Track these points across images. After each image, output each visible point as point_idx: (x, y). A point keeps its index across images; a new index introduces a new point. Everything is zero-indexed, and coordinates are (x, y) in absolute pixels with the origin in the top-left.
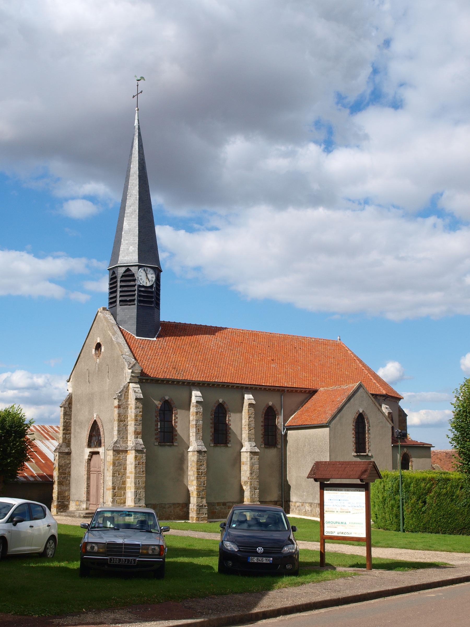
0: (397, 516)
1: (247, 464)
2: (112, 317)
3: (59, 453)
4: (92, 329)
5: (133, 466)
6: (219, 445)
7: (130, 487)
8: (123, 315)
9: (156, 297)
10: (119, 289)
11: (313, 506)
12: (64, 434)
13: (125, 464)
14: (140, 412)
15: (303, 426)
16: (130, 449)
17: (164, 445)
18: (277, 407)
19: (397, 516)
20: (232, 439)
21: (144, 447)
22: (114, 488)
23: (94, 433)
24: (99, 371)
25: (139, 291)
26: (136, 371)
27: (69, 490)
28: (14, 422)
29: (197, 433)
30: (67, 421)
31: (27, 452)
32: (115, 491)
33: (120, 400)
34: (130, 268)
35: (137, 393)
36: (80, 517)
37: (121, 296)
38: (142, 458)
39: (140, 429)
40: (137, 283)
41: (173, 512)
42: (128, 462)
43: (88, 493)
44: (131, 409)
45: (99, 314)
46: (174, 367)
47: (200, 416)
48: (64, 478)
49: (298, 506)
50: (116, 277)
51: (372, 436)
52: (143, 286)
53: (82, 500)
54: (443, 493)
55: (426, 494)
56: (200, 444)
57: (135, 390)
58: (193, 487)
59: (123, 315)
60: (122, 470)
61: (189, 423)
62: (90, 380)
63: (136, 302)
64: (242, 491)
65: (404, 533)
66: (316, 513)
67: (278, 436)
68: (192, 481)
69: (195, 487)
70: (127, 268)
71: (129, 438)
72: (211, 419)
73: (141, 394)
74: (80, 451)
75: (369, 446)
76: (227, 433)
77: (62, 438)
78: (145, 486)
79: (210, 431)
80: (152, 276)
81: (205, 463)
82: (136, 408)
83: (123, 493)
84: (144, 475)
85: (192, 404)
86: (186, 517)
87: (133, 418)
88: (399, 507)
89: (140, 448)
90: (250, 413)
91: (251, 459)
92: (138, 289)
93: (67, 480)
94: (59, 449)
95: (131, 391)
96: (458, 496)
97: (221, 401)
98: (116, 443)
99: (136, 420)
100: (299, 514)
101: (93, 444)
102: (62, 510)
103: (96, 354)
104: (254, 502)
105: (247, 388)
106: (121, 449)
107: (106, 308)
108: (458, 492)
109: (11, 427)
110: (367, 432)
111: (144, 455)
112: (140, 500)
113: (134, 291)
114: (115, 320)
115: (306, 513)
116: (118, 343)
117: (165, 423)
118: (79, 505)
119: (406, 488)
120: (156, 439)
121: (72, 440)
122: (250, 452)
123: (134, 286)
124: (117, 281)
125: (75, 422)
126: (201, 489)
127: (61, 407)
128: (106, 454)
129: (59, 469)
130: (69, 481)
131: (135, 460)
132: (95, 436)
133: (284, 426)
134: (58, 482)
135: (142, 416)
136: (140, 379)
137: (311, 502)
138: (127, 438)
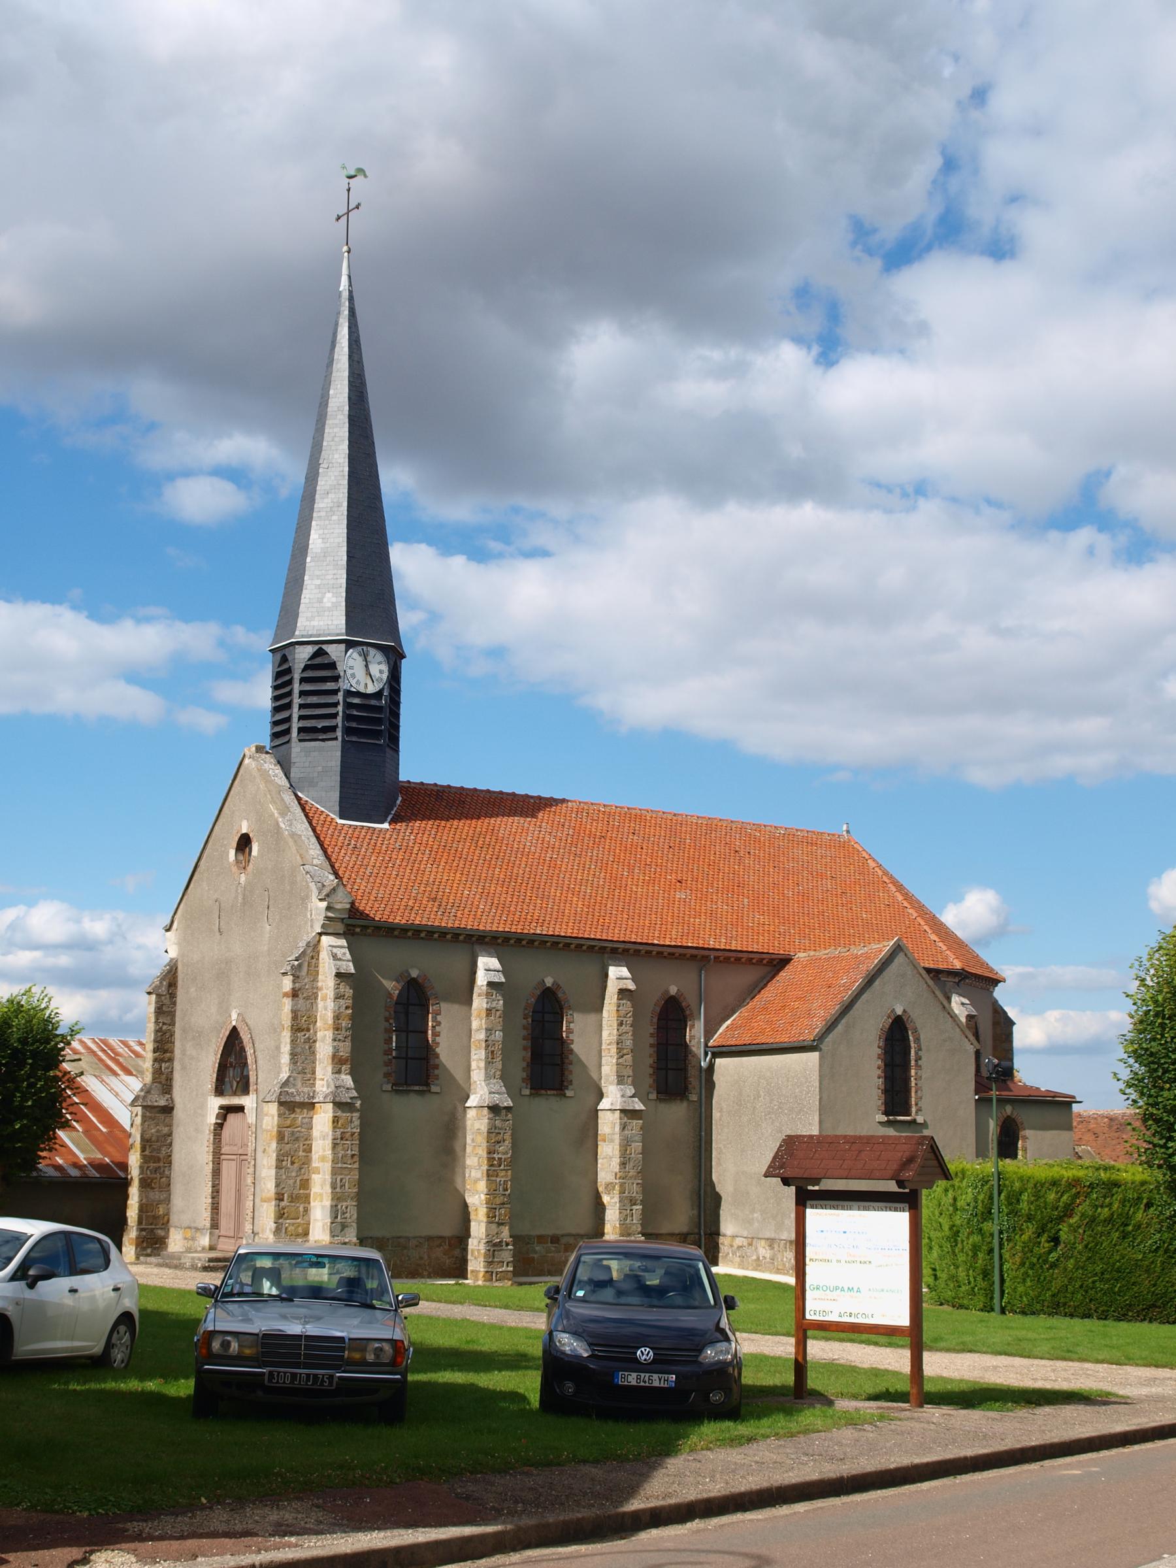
0: (986, 1274)
1: (612, 1141)
2: (278, 771)
3: (144, 1107)
5: (328, 1143)
6: (543, 1092)
7: (321, 1195)
8: (307, 764)
10: (297, 701)
11: (776, 1246)
12: (155, 1060)
13: (308, 1138)
14: (347, 1008)
15: (753, 1047)
16: (321, 1099)
17: (407, 1092)
18: (690, 999)
19: (986, 1274)
20: (575, 1076)
21: (356, 1094)
22: (279, 1197)
23: (232, 1059)
24: (244, 904)
25: (348, 705)
26: (338, 906)
27: (168, 1200)
28: (32, 1031)
29: (489, 1062)
30: (165, 1027)
31: (64, 1105)
32: (283, 1204)
33: (296, 978)
34: (324, 647)
35: (340, 960)
36: (194, 1268)
37: (301, 718)
38: (351, 1121)
39: (345, 1049)
40: (344, 685)
41: (426, 1257)
42: (316, 1133)
43: (215, 1208)
44: (324, 999)
45: (247, 761)
46: (433, 896)
47: (496, 1018)
48: (156, 1170)
49: (739, 1247)
50: (289, 671)
51: (925, 1074)
52: (358, 694)
53: (200, 1226)
54: (1102, 1217)
55: (1060, 1219)
56: (496, 1088)
57: (334, 955)
58: (477, 1197)
59: (307, 764)
60: (301, 1153)
61: (470, 1037)
62: (223, 927)
63: (339, 733)
64: (599, 1208)
65: (1003, 1317)
66: (784, 1265)
67: (692, 1072)
68: (476, 1181)
69: (483, 1197)
70: (317, 647)
71: (319, 1073)
72: (525, 1028)
73: (351, 964)
74: (197, 1103)
75: (919, 1099)
76: (563, 1063)
77: (151, 1070)
78: (358, 1194)
79: (521, 1057)
80: (380, 669)
81: (508, 1136)
82: (338, 997)
83: (301, 1209)
84: (356, 1166)
85: (476, 989)
86: (459, 1270)
87: (330, 1022)
88: (991, 1251)
89: (345, 1098)
90: (622, 1013)
91: (624, 1127)
92: (344, 701)
93: (162, 1175)
94: (144, 1098)
95: (324, 956)
96: (1138, 1227)
97: (549, 982)
98: (286, 1083)
99: (337, 1028)
100: (742, 1266)
101: (228, 1086)
102: (149, 1251)
103: (237, 861)
104: (629, 1235)
105: (614, 951)
106: (298, 1099)
107: (264, 747)
108: (1139, 1215)
109: (23, 1041)
110: (913, 1063)
111: (357, 1115)
112: (344, 1226)
114: (288, 778)
115: (758, 1265)
116: (293, 835)
118: (193, 1239)
119: (1010, 1204)
120: (386, 1075)
121: (177, 1076)
122: (621, 1111)
123: (338, 690)
125: (184, 1030)
126: (498, 1200)
127: (149, 993)
128: (260, 1113)
129: (143, 1149)
130: (169, 1177)
131: (334, 1128)
132: (233, 1068)
133: (706, 1046)
134: (140, 1180)
135: (352, 1018)
136: (347, 925)
137: (773, 1236)
138: (314, 1073)
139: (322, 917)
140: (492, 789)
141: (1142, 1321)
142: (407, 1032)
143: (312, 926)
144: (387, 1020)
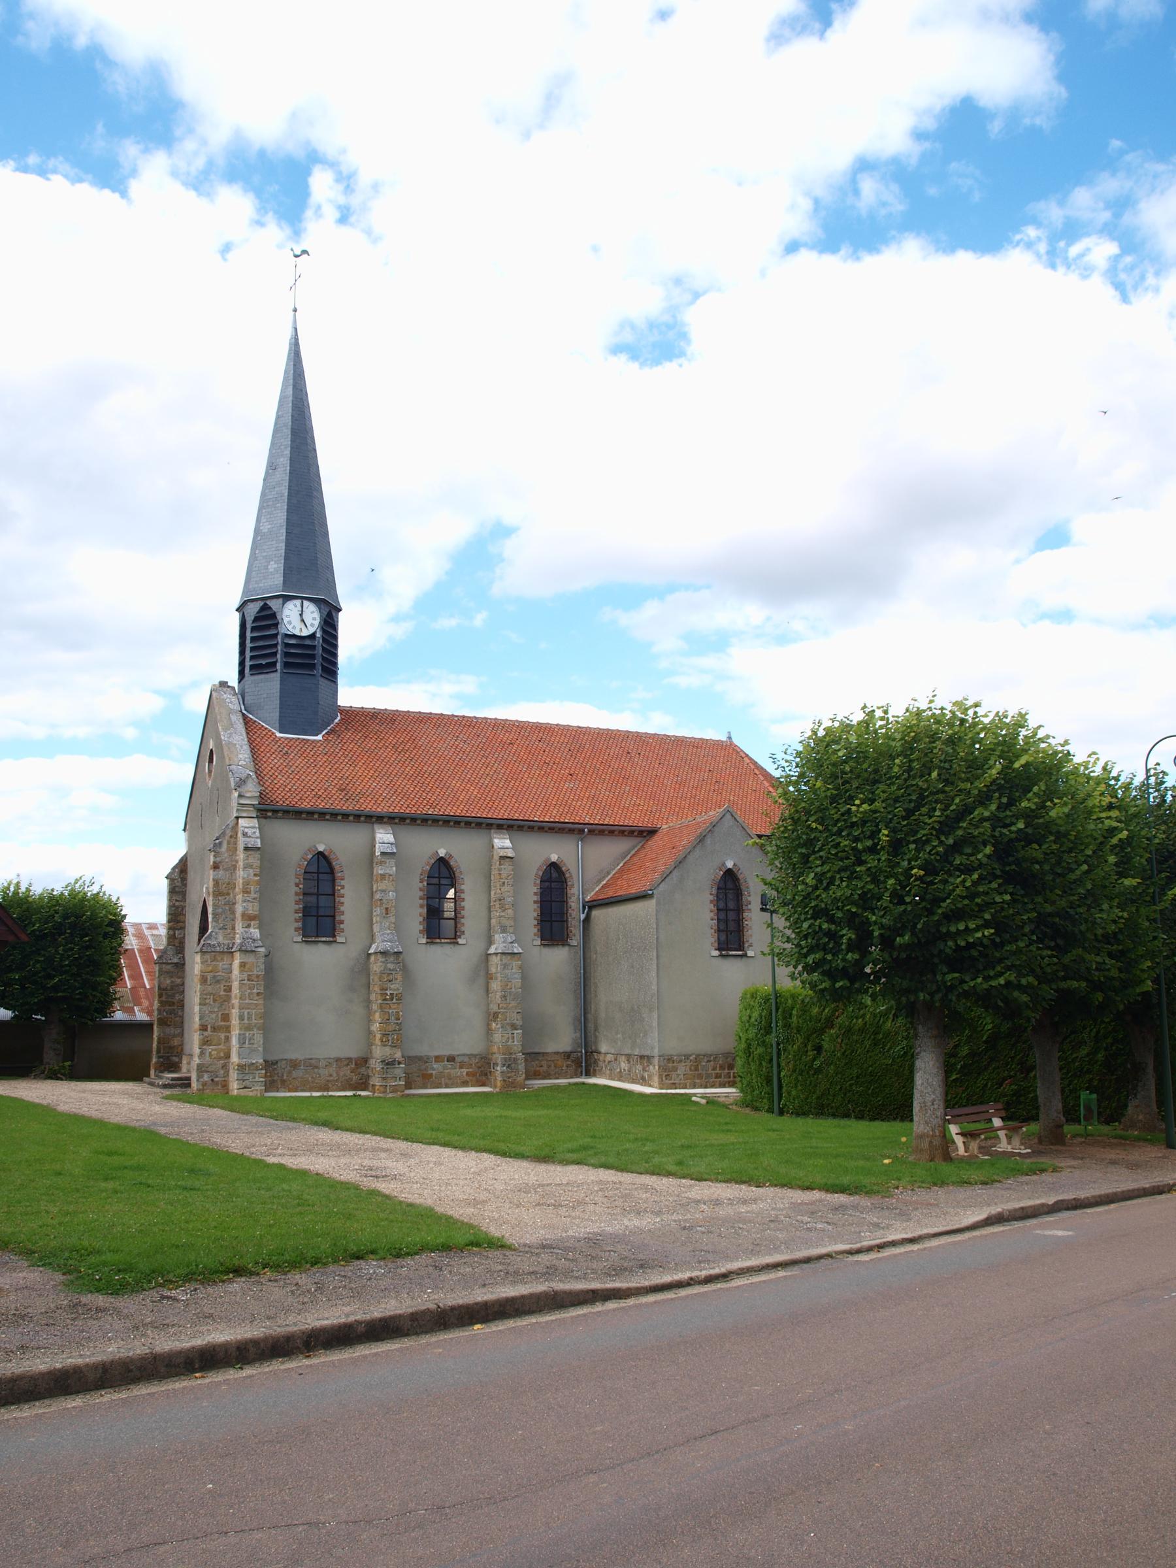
0: (769, 1081)
14: (255, 875)
19: (769, 1081)
26: (248, 795)
27: (182, 1035)
40: (282, 630)
52: (294, 636)
54: (856, 1028)
55: (822, 1031)
72: (421, 890)
88: (771, 1060)
96: (887, 1034)
97: (442, 853)
108: (889, 1024)
117: (452, 922)
119: (785, 1018)
123: (276, 635)
130: (182, 1017)
136: (259, 810)
141: (895, 1119)
142: (551, 921)
144: (297, 885)
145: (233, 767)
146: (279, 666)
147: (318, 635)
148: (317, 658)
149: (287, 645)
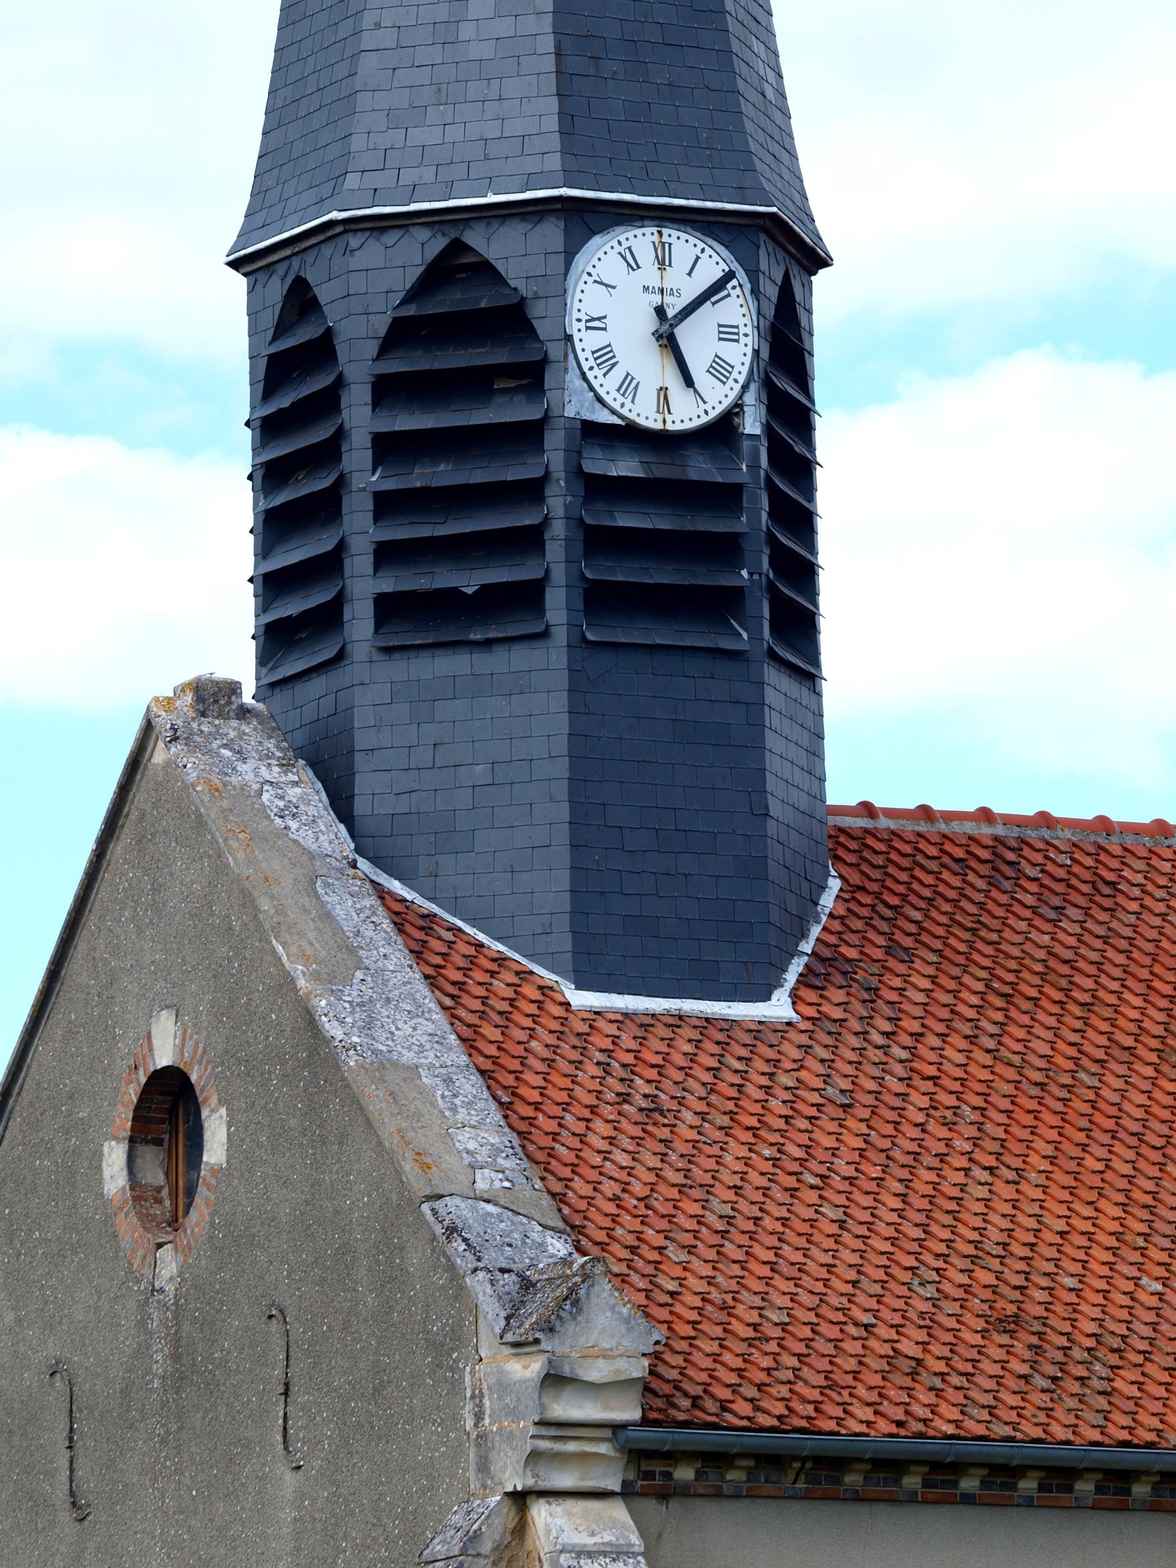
2: (304, 792)
4: (91, 922)
9: (777, 499)
10: (363, 476)
24: (178, 1379)
26: (596, 1372)
37: (387, 555)
45: (159, 755)
50: (323, 350)
52: (629, 435)
59: (423, 756)
62: (88, 1481)
63: (558, 606)
70: (439, 244)
92: (577, 472)
107: (233, 688)
113: (534, 490)
116: (383, 1065)
123: (531, 435)
124: (340, 434)
136: (636, 1455)
139: (526, 1425)
140: (1117, 816)
143: (484, 1467)
145: (457, 1208)
146: (558, 606)
147: (752, 424)
148: (712, 553)
149: (599, 488)
